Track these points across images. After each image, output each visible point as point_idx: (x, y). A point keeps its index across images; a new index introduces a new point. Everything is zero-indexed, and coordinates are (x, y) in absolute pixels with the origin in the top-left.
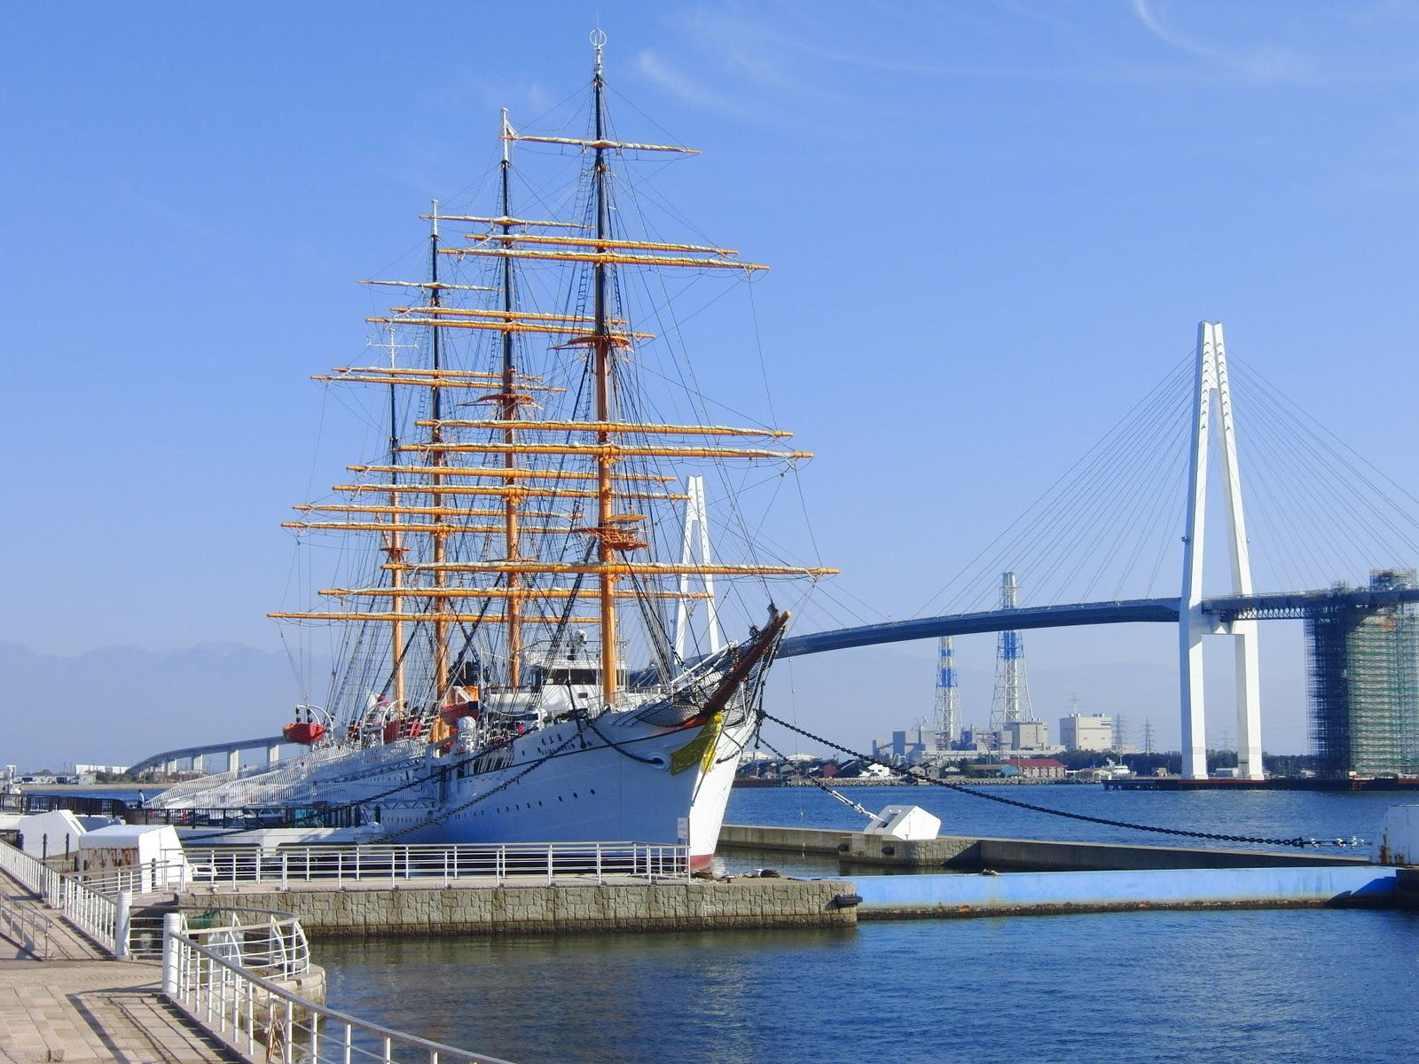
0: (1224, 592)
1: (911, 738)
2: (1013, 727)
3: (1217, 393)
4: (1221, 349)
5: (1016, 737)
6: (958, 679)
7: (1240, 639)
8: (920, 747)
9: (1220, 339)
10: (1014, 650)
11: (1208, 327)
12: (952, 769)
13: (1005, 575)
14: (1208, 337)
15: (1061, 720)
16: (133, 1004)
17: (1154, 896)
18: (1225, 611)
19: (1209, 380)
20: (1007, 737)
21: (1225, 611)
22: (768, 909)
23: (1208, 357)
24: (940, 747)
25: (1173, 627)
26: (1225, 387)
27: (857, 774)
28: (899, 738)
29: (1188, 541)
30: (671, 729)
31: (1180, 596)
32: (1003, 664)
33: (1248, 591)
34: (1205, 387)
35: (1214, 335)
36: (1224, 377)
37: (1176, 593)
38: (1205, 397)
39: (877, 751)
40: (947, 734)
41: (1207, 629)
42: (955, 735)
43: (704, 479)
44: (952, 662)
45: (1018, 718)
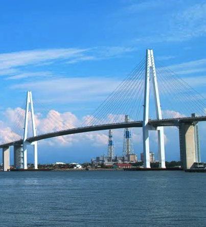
0: (154, 118)
1: (101, 159)
2: (128, 156)
3: (151, 68)
4: (152, 56)
5: (129, 158)
6: (114, 143)
7: (159, 131)
8: (103, 161)
9: (152, 54)
10: (128, 135)
11: (149, 51)
13: (126, 116)
14: (29, 94)
18: (154, 124)
19: (149, 64)
20: (126, 158)
21: (154, 124)
23: (149, 59)
24: (109, 161)
26: (154, 66)
27: (73, 167)
28: (98, 159)
29: (145, 106)
32: (126, 139)
34: (149, 66)
35: (150, 53)
36: (154, 64)
37: (141, 119)
38: (148, 69)
39: (92, 162)
42: (113, 157)
43: (153, 51)
44: (112, 139)
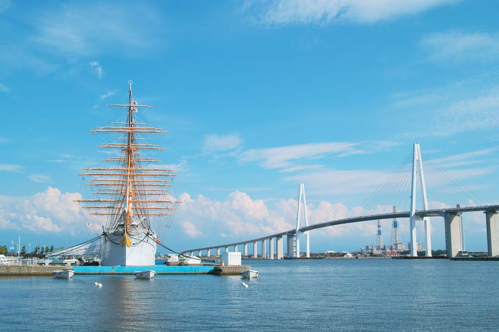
0: (421, 209)
1: (370, 248)
2: (396, 245)
4: (419, 150)
5: (397, 247)
7: (425, 221)
9: (419, 147)
10: (394, 224)
12: (368, 255)
14: (416, 147)
15: (408, 243)
16: (348, 277)
17: (88, 272)
18: (421, 215)
19: (416, 158)
20: (394, 247)
21: (421, 215)
22: (47, 272)
24: (377, 249)
25: (408, 219)
28: (367, 248)
29: (412, 197)
30: (196, 258)
31: (127, 264)
32: (394, 229)
33: (427, 209)
35: (417, 147)
36: (420, 157)
37: (409, 210)
38: (415, 162)
40: (379, 247)
41: (421, 219)
42: (382, 247)
44: (381, 229)
45: (397, 242)
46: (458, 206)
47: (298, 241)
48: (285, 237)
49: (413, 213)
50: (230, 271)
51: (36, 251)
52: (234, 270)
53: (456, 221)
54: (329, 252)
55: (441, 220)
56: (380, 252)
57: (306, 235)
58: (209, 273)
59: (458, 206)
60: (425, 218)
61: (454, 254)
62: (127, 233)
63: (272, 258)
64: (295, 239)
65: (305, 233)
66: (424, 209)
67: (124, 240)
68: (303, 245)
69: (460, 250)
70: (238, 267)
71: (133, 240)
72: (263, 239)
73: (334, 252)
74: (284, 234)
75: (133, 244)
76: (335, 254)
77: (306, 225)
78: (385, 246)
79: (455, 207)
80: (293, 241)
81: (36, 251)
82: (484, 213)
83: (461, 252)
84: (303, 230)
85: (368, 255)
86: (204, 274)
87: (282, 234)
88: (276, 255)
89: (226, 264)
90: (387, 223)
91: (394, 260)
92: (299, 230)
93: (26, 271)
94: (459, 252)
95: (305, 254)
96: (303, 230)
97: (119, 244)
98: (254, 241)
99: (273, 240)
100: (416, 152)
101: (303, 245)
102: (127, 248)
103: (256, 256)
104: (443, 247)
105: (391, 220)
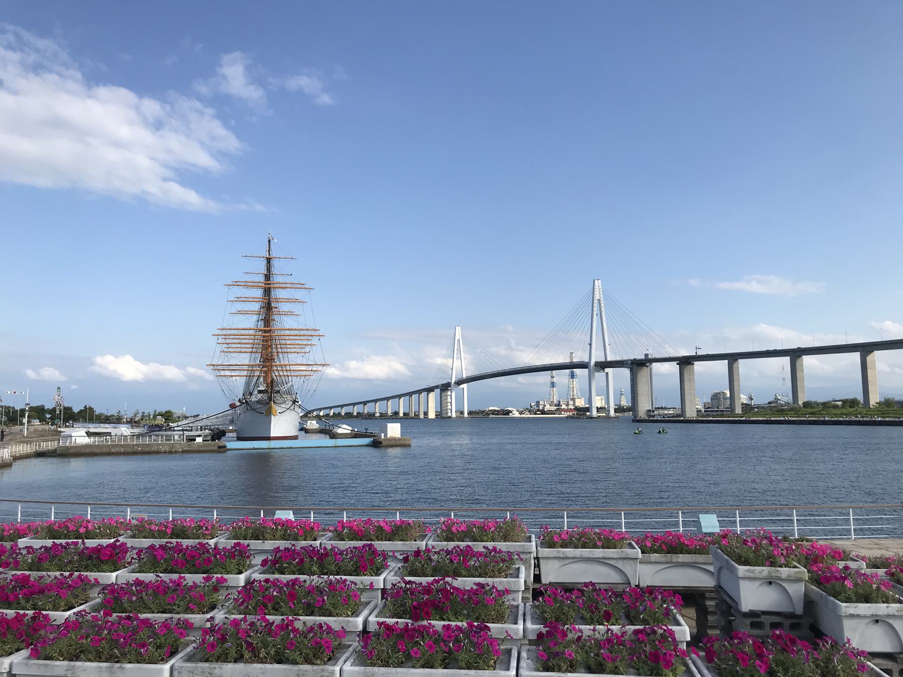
7: (607, 373)
9: (600, 284)
19: (597, 296)
21: (602, 366)
24: (550, 406)
46: (646, 355)
47: (453, 394)
48: (438, 391)
49: (593, 363)
50: (391, 443)
51: (135, 416)
52: (393, 443)
53: (643, 374)
54: (490, 408)
55: (626, 372)
56: (554, 408)
57: (463, 388)
58: (367, 446)
59: (646, 355)
60: (607, 370)
61: (642, 413)
62: (274, 401)
63: (422, 416)
64: (449, 393)
65: (462, 386)
66: (606, 358)
67: (270, 408)
68: (460, 400)
69: (648, 409)
70: (399, 439)
71: (279, 408)
72: (410, 394)
73: (496, 409)
74: (437, 387)
75: (279, 413)
76: (498, 411)
77: (462, 376)
78: (559, 402)
79: (643, 357)
80: (447, 396)
81: (135, 416)
82: (677, 364)
83: (649, 411)
84: (459, 383)
85: (539, 412)
86: (362, 446)
87: (433, 387)
88: (426, 414)
89: (386, 435)
90: (561, 377)
91: (569, 420)
92: (455, 383)
93: (154, 449)
94: (648, 410)
95: (462, 413)
96: (459, 383)
97: (263, 413)
98: (399, 396)
99: (424, 394)
100: (597, 290)
101: (460, 400)
102: (272, 416)
103: (401, 415)
104: (625, 402)
105: (568, 371)
